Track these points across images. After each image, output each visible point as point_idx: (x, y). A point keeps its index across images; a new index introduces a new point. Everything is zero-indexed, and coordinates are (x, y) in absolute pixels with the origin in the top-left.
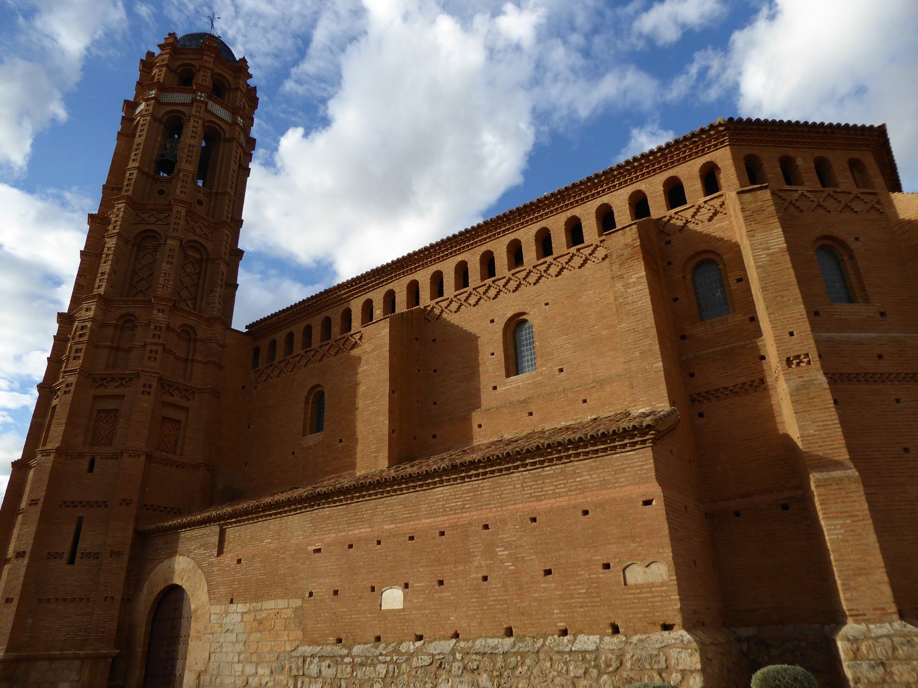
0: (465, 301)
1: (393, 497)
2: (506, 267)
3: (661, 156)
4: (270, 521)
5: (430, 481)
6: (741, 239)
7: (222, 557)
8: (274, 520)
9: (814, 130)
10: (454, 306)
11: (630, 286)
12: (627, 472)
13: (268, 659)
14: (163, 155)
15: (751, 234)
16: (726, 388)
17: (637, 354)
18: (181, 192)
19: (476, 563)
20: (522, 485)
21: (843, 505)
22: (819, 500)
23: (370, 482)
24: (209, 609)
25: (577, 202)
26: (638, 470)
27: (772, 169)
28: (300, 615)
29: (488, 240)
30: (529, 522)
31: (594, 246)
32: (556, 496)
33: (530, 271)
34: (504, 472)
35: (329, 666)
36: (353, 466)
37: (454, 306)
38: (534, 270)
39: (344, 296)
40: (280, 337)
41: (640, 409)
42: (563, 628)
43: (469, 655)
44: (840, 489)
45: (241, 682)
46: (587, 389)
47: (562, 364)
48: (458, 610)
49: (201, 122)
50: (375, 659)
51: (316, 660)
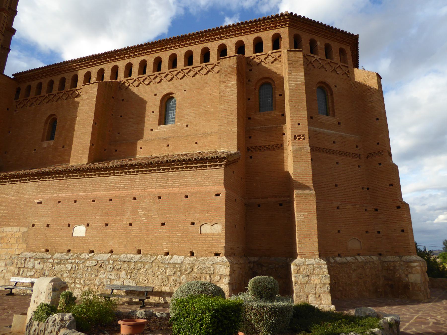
0: (143, 81)
2: (167, 67)
3: (255, 25)
5: (108, 172)
6: (285, 75)
9: (328, 29)
10: (136, 83)
11: (228, 87)
12: (210, 179)
13: (5, 258)
15: (290, 73)
16: (265, 146)
17: (226, 122)
19: (127, 217)
20: (156, 180)
21: (306, 206)
22: (296, 203)
23: (74, 169)
25: (209, 40)
26: (216, 179)
27: (306, 44)
28: (25, 237)
29: (159, 51)
30: (157, 198)
31: (214, 65)
32: (173, 187)
33: (179, 72)
34: (148, 172)
35: (39, 263)
36: (68, 161)
37: (136, 83)
38: (182, 72)
40: (34, 84)
41: (222, 150)
42: (167, 252)
43: (117, 262)
44: (305, 198)
46: (198, 137)
47: (188, 123)
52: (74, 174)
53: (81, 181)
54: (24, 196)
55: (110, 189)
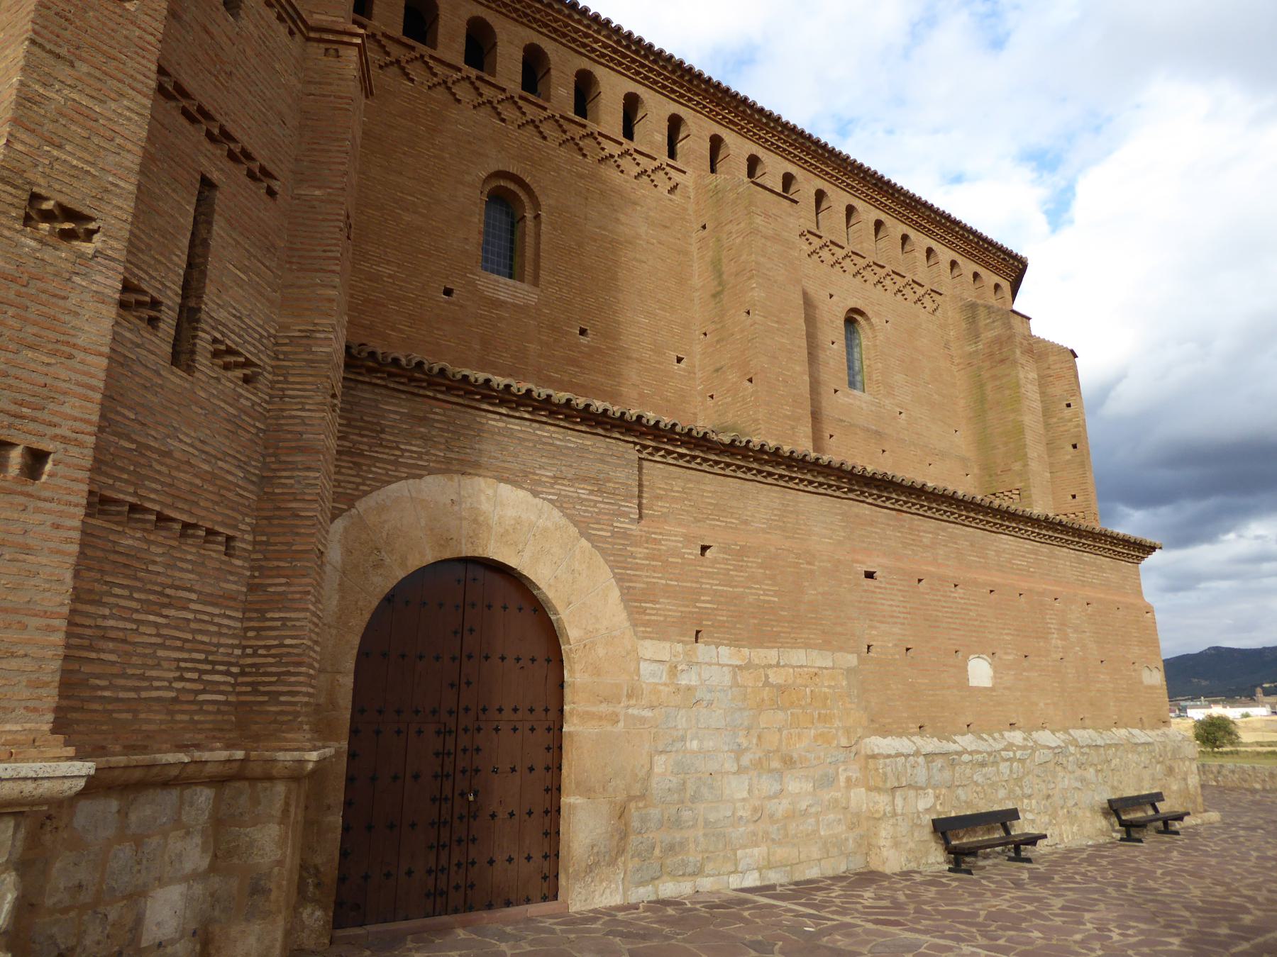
29: (544, 30)
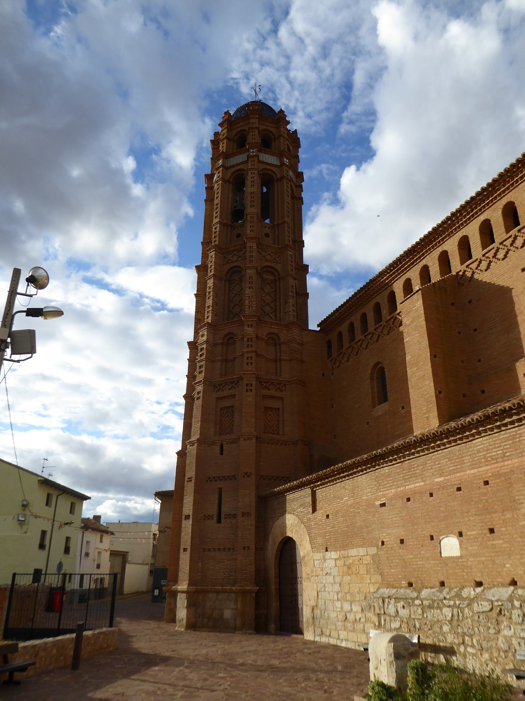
1: (439, 452)
4: (345, 482)
5: (467, 433)
7: (316, 514)
8: (348, 480)
14: (235, 207)
18: (250, 231)
24: (313, 556)
29: (507, 192)
35: (404, 607)
39: (387, 281)
40: (344, 328)
45: (341, 617)
48: (512, 557)
49: (256, 172)
50: (440, 603)
51: (393, 601)
52: (419, 449)
53: (431, 459)
54: (361, 498)
55: (481, 462)
